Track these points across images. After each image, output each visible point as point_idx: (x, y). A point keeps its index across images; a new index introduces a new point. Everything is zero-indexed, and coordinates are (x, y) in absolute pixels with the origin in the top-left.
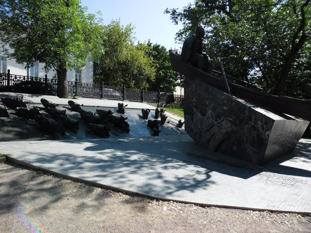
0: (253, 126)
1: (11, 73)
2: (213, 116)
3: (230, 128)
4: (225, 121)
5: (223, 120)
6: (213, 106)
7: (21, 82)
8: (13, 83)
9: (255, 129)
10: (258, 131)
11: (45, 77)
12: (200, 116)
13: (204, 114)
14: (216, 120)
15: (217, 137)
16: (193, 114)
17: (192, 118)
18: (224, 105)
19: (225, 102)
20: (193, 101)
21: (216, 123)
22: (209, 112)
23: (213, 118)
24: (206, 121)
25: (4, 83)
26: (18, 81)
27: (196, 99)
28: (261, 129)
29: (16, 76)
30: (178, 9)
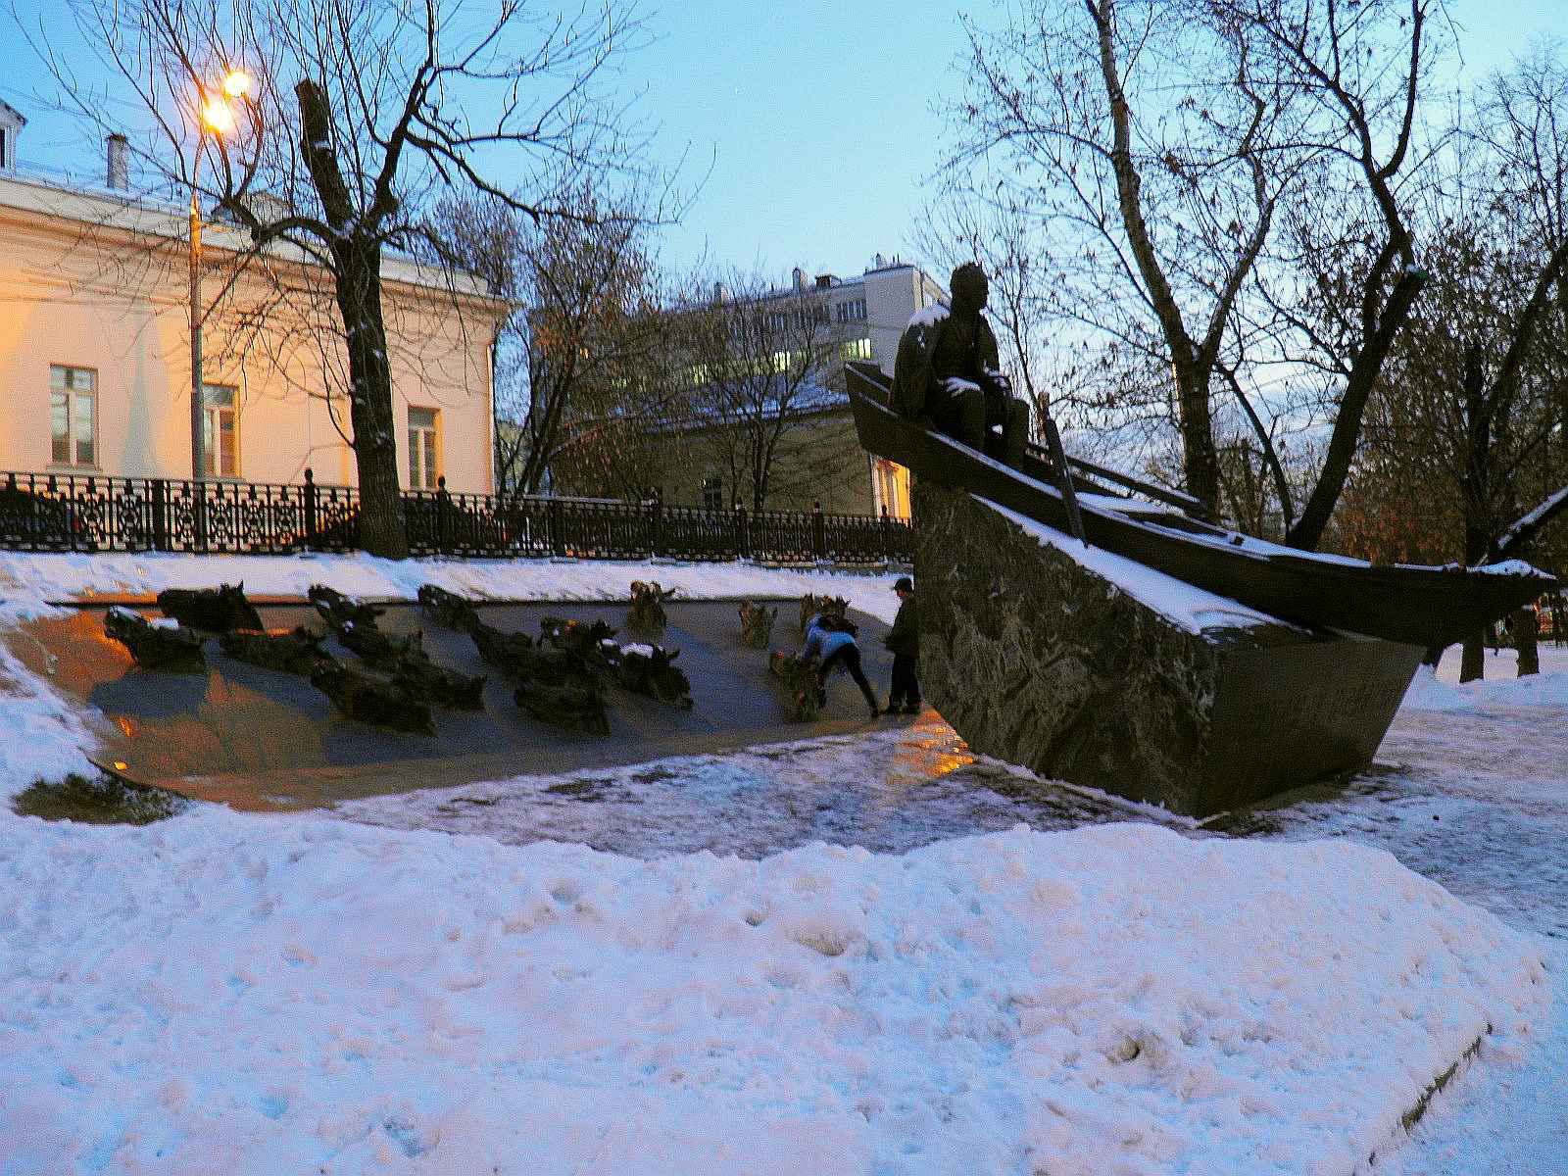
0: (1158, 675)
1: (448, 487)
2: (1026, 639)
3: (1084, 685)
4: (1068, 660)
5: (1062, 656)
6: (1026, 602)
7: (352, 513)
8: (326, 521)
9: (1164, 685)
10: (1176, 693)
11: (303, 481)
12: (977, 639)
13: (993, 632)
14: (1039, 656)
15: (1044, 720)
16: (954, 631)
17: (950, 645)
18: (1062, 596)
19: (1066, 585)
20: (949, 577)
21: (1037, 665)
22: (1013, 624)
23: (1025, 647)
24: (1002, 660)
25: (140, 521)
26: (342, 510)
27: (960, 570)
28: (1184, 688)
29: (129, 481)
30: (295, 858)
